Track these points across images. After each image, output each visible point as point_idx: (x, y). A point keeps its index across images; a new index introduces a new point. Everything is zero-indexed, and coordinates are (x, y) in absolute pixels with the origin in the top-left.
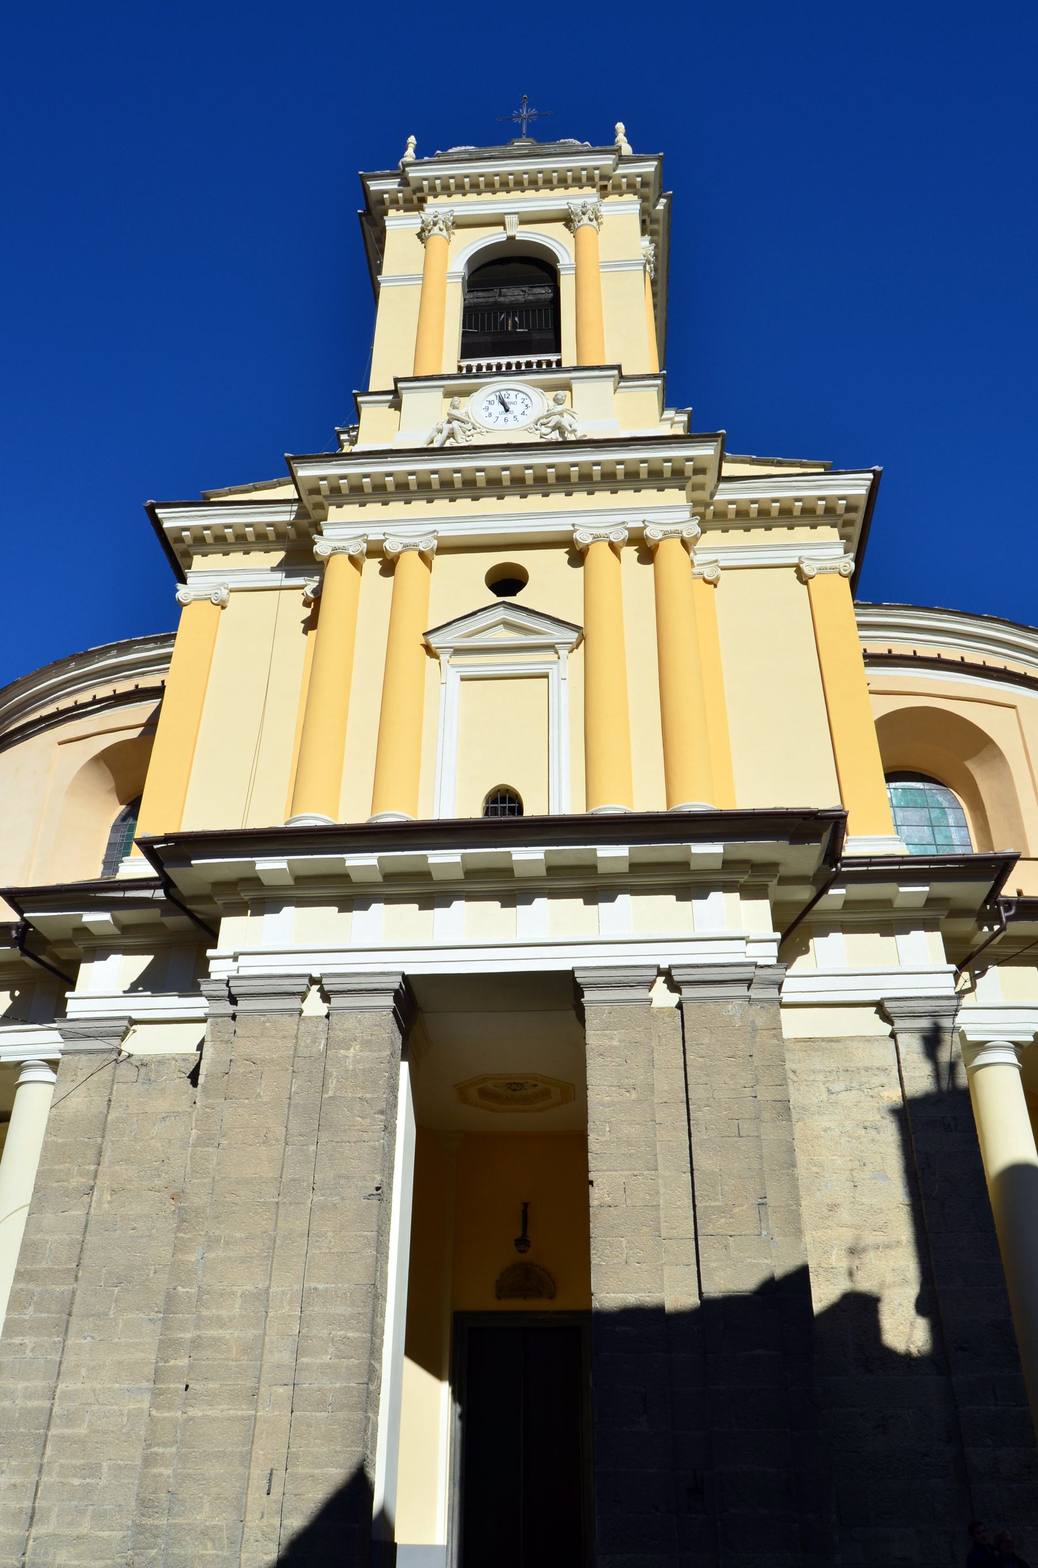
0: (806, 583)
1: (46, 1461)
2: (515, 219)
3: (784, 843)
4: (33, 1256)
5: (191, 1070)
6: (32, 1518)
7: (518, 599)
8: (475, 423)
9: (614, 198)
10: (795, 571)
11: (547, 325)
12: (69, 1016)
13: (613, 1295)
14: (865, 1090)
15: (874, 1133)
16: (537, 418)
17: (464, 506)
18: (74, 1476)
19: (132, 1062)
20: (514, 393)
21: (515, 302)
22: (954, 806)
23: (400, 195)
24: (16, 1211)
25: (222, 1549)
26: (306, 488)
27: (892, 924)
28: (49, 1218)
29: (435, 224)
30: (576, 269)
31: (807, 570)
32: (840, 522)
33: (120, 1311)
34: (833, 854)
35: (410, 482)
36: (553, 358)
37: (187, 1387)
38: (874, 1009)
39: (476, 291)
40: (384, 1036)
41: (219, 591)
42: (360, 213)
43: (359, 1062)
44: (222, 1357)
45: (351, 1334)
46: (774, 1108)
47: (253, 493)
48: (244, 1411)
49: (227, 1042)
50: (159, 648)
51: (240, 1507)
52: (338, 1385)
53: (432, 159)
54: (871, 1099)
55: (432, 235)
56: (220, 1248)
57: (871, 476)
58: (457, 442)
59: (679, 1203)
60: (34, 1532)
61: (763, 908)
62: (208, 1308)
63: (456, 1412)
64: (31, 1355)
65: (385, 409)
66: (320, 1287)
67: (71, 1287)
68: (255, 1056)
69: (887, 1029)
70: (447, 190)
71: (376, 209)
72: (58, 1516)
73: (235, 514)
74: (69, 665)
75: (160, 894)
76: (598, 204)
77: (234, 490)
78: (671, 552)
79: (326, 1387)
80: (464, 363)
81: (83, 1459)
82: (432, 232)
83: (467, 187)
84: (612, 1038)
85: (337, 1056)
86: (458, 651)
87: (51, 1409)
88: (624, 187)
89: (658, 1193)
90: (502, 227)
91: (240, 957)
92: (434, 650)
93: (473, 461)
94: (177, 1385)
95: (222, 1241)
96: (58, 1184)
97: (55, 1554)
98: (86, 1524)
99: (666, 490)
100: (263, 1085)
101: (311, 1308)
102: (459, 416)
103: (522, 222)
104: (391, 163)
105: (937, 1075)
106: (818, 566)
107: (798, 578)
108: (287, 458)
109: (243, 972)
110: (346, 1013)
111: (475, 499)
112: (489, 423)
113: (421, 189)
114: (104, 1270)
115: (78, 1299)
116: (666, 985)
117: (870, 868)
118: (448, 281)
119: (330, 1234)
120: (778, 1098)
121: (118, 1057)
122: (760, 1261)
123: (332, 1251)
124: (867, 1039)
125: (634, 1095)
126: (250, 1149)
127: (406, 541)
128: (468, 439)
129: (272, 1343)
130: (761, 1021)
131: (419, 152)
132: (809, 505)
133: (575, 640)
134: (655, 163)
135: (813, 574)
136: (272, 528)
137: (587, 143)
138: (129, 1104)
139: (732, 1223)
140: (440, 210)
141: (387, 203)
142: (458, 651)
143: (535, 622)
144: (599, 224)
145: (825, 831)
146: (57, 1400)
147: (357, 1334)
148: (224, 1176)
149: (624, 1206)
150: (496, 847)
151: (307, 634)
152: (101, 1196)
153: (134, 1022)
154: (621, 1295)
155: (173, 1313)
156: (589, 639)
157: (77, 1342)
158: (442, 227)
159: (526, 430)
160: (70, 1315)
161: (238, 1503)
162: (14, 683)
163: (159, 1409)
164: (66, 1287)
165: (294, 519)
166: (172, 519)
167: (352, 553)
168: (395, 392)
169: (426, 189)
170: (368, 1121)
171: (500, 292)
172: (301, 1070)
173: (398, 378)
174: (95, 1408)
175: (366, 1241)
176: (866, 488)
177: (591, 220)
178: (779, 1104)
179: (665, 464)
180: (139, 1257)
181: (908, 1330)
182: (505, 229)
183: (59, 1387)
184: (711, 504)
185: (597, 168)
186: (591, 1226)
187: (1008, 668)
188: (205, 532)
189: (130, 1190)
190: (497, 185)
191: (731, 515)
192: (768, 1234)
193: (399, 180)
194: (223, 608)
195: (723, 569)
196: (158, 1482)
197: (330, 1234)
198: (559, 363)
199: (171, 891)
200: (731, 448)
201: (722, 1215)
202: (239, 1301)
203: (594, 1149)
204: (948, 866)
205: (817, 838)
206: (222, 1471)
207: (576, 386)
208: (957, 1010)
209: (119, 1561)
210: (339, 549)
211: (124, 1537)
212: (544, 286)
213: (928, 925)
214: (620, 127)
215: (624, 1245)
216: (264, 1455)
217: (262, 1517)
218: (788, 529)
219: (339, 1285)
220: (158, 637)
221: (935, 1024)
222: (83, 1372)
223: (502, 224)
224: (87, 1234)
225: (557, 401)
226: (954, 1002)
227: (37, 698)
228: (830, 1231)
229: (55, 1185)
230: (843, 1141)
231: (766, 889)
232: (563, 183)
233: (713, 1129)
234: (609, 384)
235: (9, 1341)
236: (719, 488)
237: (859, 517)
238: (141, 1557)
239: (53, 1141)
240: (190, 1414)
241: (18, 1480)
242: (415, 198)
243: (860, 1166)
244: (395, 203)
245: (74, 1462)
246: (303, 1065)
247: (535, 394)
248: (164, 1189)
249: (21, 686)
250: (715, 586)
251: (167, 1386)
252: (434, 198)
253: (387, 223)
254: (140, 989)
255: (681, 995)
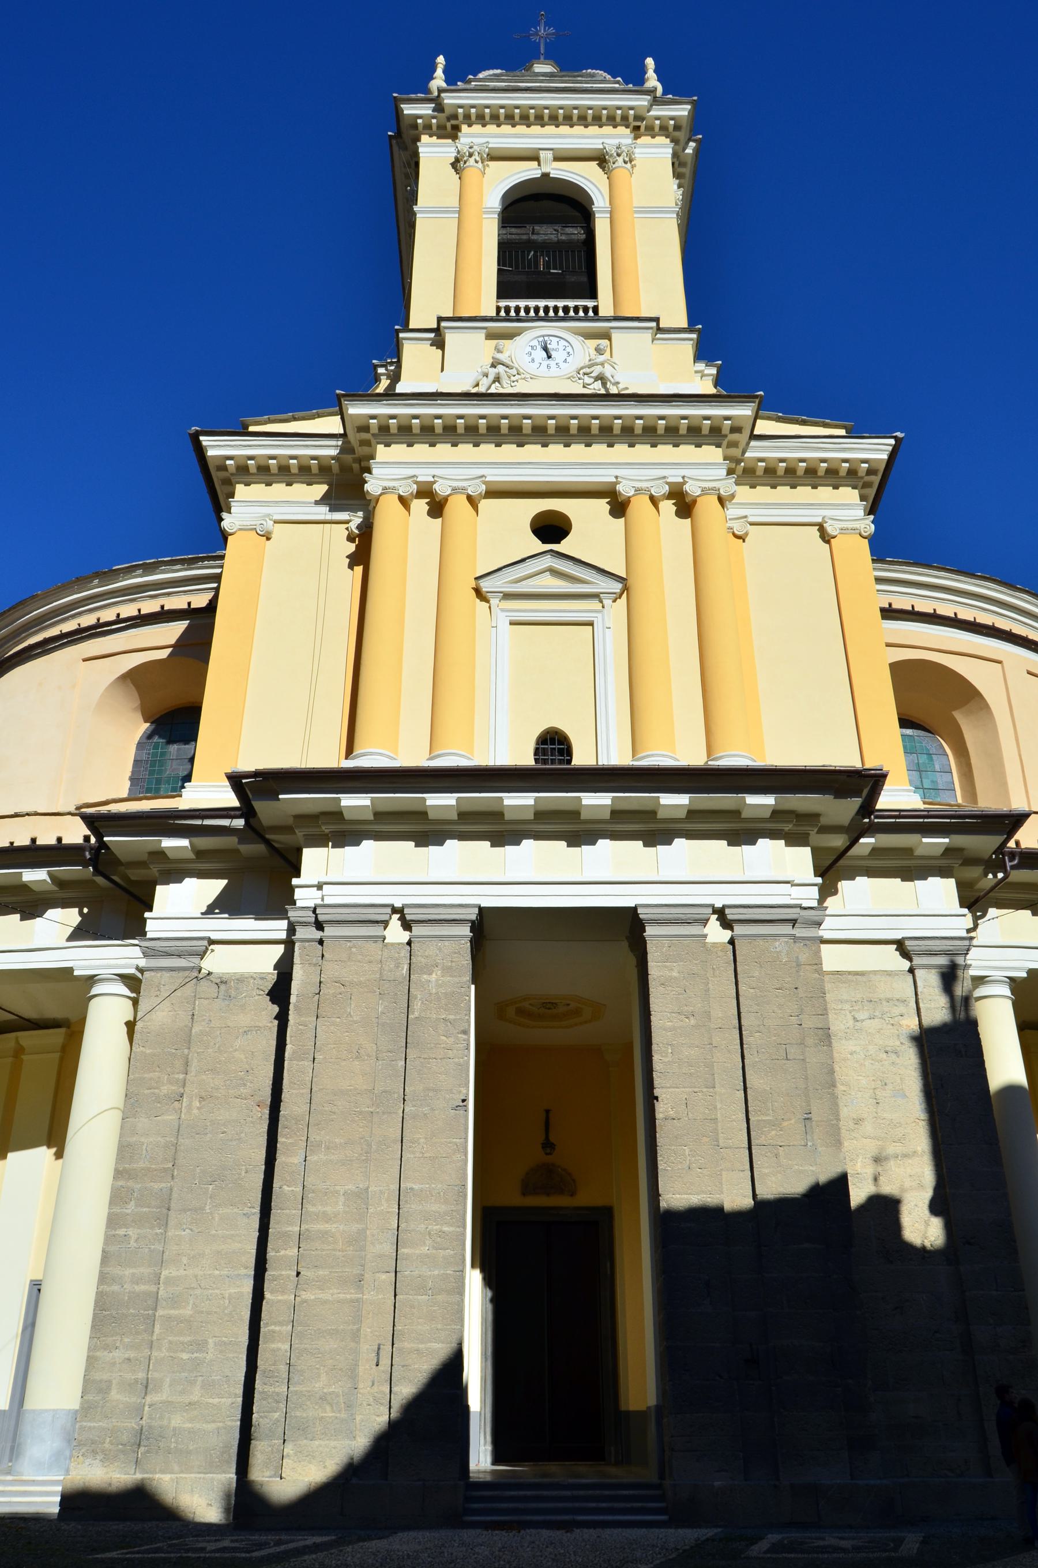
0: (828, 542)
1: (155, 1337)
2: (550, 155)
3: (829, 798)
4: (131, 1156)
5: (270, 988)
6: (146, 1387)
7: (563, 547)
8: (519, 368)
9: (645, 140)
10: (818, 530)
11: (580, 267)
12: (149, 935)
13: (678, 1196)
14: (887, 1019)
15: (894, 1056)
16: (579, 368)
17: (509, 451)
18: (182, 1351)
19: (212, 979)
20: (556, 339)
21: (548, 241)
22: (940, 753)
23: (434, 121)
24: (99, 1114)
25: (340, 1411)
26: (355, 425)
27: (911, 870)
28: (142, 1122)
29: (471, 155)
30: (611, 212)
31: (830, 529)
32: (861, 484)
33: (216, 1206)
34: (868, 808)
35: (458, 425)
36: (590, 304)
37: (298, 1274)
38: (895, 946)
39: (510, 227)
40: (463, 962)
41: (264, 523)
42: (390, 136)
43: (440, 986)
44: (329, 1247)
45: (446, 1229)
46: (816, 1035)
47: (292, 423)
48: (352, 1295)
49: (315, 965)
50: (186, 570)
51: (353, 1374)
52: (436, 1272)
53: (467, 86)
54: (891, 1027)
55: (468, 167)
56: (322, 1151)
57: (892, 441)
58: (502, 387)
59: (734, 1117)
60: (148, 1399)
61: (803, 855)
62: (314, 1205)
63: (486, 1295)
64: (135, 1245)
65: (426, 346)
66: (416, 1187)
67: (169, 1185)
68: (344, 979)
69: (906, 964)
70: (481, 120)
71: (408, 133)
72: (170, 1385)
73: (280, 446)
74: (92, 582)
75: (239, 823)
76: (633, 146)
77: (273, 418)
78: (707, 508)
79: (425, 1274)
80: (503, 303)
81: (189, 1336)
82: (467, 164)
83: (502, 118)
84: (672, 970)
85: (420, 981)
86: (507, 596)
87: (158, 1293)
88: (657, 129)
89: (715, 1108)
90: (536, 163)
91: (325, 887)
92: (484, 594)
93: (521, 408)
94: (288, 1272)
95: (323, 1146)
96: (149, 1091)
97: (169, 1419)
98: (197, 1393)
99: (703, 446)
100: (353, 1006)
101: (409, 1206)
102: (505, 361)
103: (557, 159)
104: (419, 85)
105: (953, 1007)
106: (840, 526)
107: (820, 537)
108: (338, 395)
109: (328, 901)
110: (427, 941)
111: (520, 445)
112: (532, 368)
113: (455, 116)
114: (198, 1170)
115: (175, 1195)
116: (718, 923)
117: (897, 820)
118: (484, 216)
119: (422, 1140)
120: (820, 1026)
121: (199, 976)
122: (807, 1168)
123: (425, 1155)
124: (889, 974)
125: (693, 1022)
126: (343, 1063)
127: (455, 484)
128: (513, 384)
129: (373, 1236)
130: (803, 957)
131: (451, 78)
132: (834, 466)
133: (619, 591)
134: (689, 107)
135: (834, 533)
136: (316, 462)
137: (619, 79)
138: (211, 1019)
139: (782, 1135)
140: (477, 141)
141: (420, 128)
142: (507, 596)
143: (561, 563)
144: (633, 167)
145: (866, 787)
146: (161, 1285)
147: (451, 1229)
148: (321, 1087)
149: (687, 1119)
150: (567, 792)
151: (352, 570)
152: (191, 1102)
153: (212, 942)
154: (686, 1196)
155: (280, 1209)
156: (633, 592)
157: (177, 1233)
158: (478, 159)
159: (569, 378)
160: (169, 1209)
161: (352, 1373)
162: (33, 597)
163: (273, 1293)
164: (163, 1185)
165: (338, 454)
166: (216, 447)
167: (402, 494)
168: (437, 331)
169: (461, 117)
170: (452, 1039)
171: (533, 229)
172: (386, 992)
173: (441, 317)
174: (198, 1292)
175: (455, 1147)
176: (888, 453)
177: (625, 162)
178: (820, 1032)
179: (705, 422)
180: (231, 1158)
181: (923, 1227)
182: (539, 165)
183: (163, 1273)
184: (741, 461)
185: (631, 108)
186: (657, 1136)
187: (996, 625)
188: (249, 462)
189: (217, 1098)
190: (532, 118)
191: (760, 472)
192: (813, 1144)
193: (434, 105)
194: (268, 539)
195: (752, 524)
196: (277, 1356)
197: (422, 1140)
198: (596, 310)
199: (252, 821)
200: (766, 408)
201: (773, 1128)
202: (342, 1199)
203: (658, 1068)
204: (967, 820)
205: (858, 794)
206: (335, 1346)
207: (615, 336)
208: (968, 950)
209: (229, 1423)
210: (389, 489)
211: (232, 1403)
212: (577, 227)
213: (943, 872)
214: (650, 62)
215: (687, 1153)
216: (371, 1332)
217: (373, 1385)
218: (812, 488)
219: (433, 1186)
220: (185, 558)
221: (952, 961)
222: (185, 1260)
223: (536, 158)
224: (180, 1137)
225: (599, 351)
226: (966, 943)
227: (58, 612)
228: (855, 1142)
229: (147, 1092)
230: (866, 1063)
231: (808, 837)
232: (597, 121)
233: (764, 1053)
234: (648, 336)
235: (113, 1232)
236: (750, 445)
237: (876, 479)
238: (266, 1419)
239: (142, 1052)
240: (303, 1297)
241: (131, 1354)
242: (449, 125)
243: (882, 1085)
244: (428, 128)
245: (181, 1339)
246: (388, 988)
247: (576, 341)
248: (250, 1097)
249: (39, 600)
250: (744, 541)
251: (279, 1273)
252: (469, 126)
253: (421, 150)
254: (217, 911)
255: (733, 931)
